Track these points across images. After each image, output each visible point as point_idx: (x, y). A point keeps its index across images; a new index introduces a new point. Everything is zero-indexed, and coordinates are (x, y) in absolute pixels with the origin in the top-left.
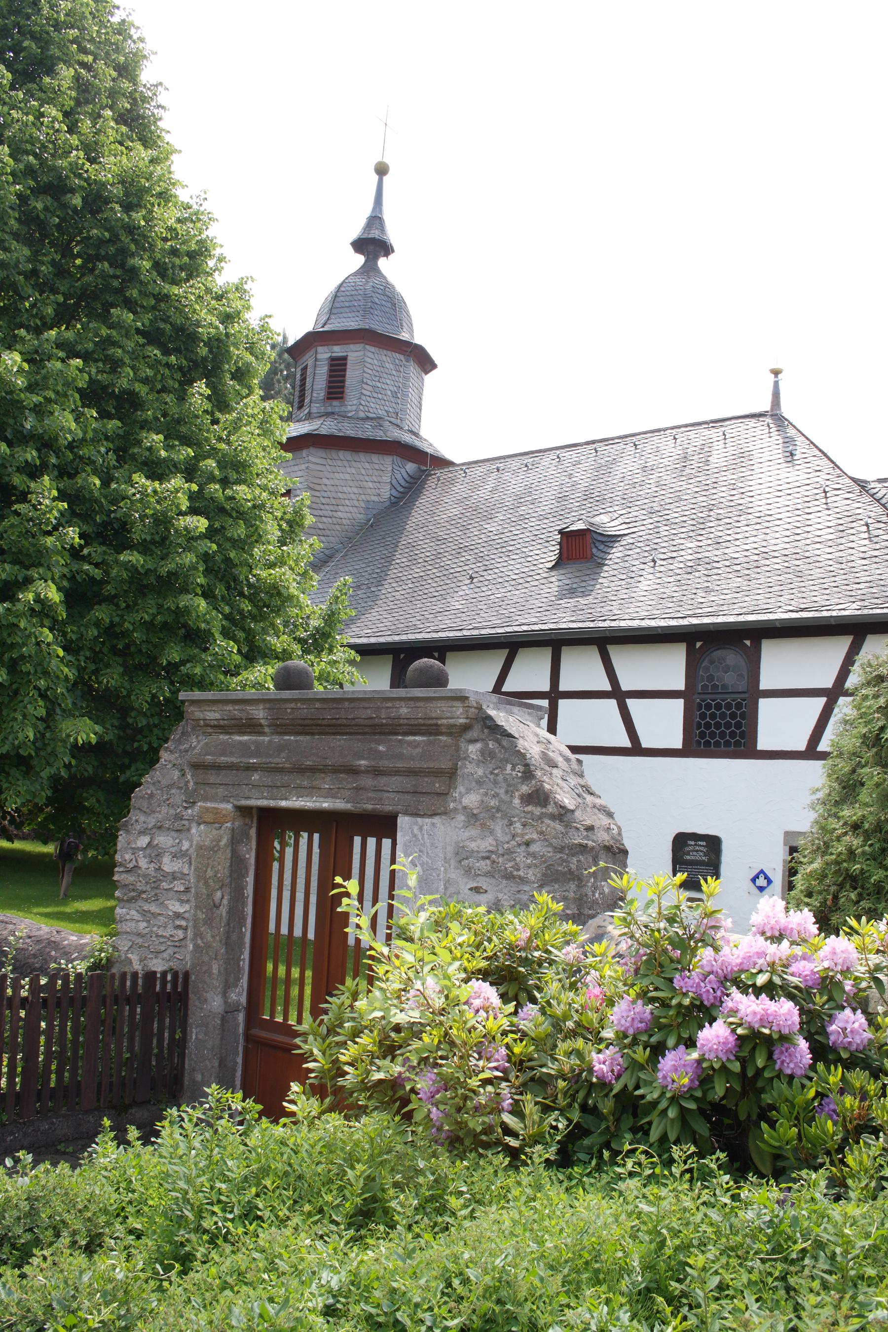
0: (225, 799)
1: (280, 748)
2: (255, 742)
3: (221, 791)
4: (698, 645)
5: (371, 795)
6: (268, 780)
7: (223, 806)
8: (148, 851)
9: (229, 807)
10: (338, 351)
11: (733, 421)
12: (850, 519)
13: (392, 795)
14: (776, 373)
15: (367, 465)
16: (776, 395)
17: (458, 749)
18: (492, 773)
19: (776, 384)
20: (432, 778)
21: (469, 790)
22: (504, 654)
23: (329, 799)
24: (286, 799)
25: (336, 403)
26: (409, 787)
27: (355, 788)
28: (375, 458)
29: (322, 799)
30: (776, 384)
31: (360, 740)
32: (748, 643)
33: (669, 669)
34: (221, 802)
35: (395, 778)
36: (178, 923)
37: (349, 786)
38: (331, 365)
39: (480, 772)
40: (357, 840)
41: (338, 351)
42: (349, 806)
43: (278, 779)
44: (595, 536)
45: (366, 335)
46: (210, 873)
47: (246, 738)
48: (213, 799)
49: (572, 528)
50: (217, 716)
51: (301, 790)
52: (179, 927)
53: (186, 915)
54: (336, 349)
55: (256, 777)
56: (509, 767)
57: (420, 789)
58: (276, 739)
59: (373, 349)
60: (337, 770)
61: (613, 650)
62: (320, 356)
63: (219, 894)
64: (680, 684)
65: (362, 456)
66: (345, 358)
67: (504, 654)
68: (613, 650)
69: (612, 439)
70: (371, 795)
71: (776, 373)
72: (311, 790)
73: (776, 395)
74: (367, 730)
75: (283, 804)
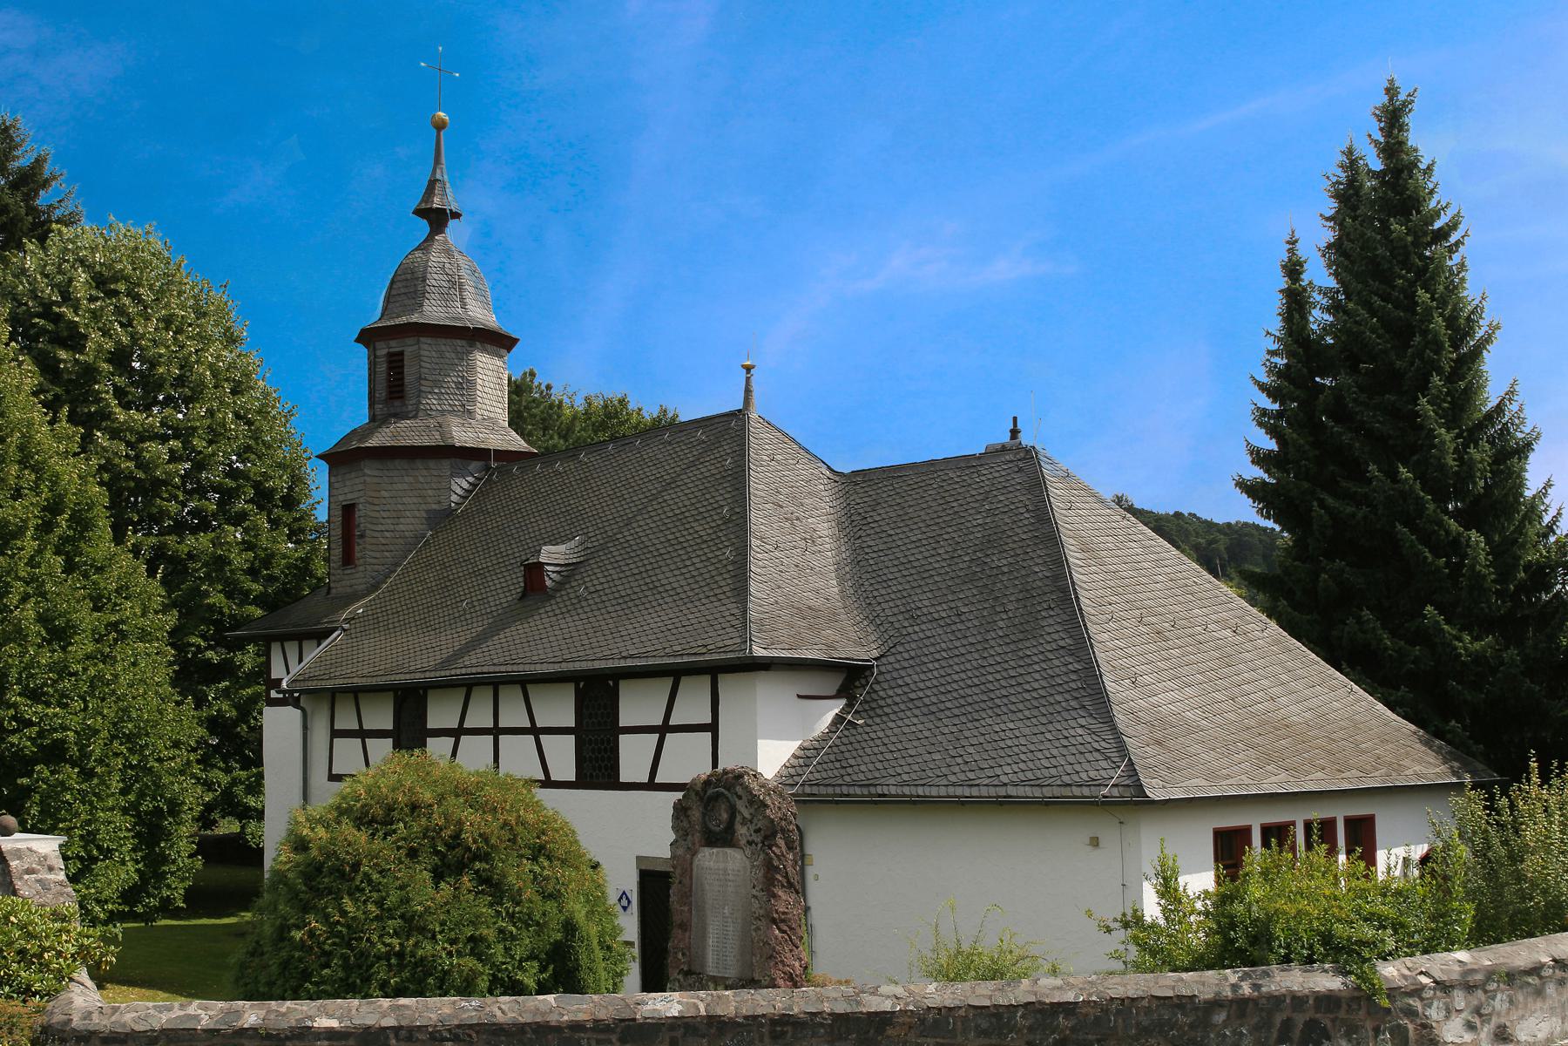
10: (395, 346)
15: (425, 473)
19: (748, 379)
22: (669, 682)
25: (397, 403)
28: (432, 464)
33: (559, 709)
38: (390, 362)
41: (395, 346)
45: (1430, 168)
54: (393, 343)
59: (429, 340)
61: (529, 687)
62: (379, 353)
64: (570, 722)
65: (419, 463)
66: (401, 353)
67: (669, 682)
68: (529, 687)
71: (748, 369)
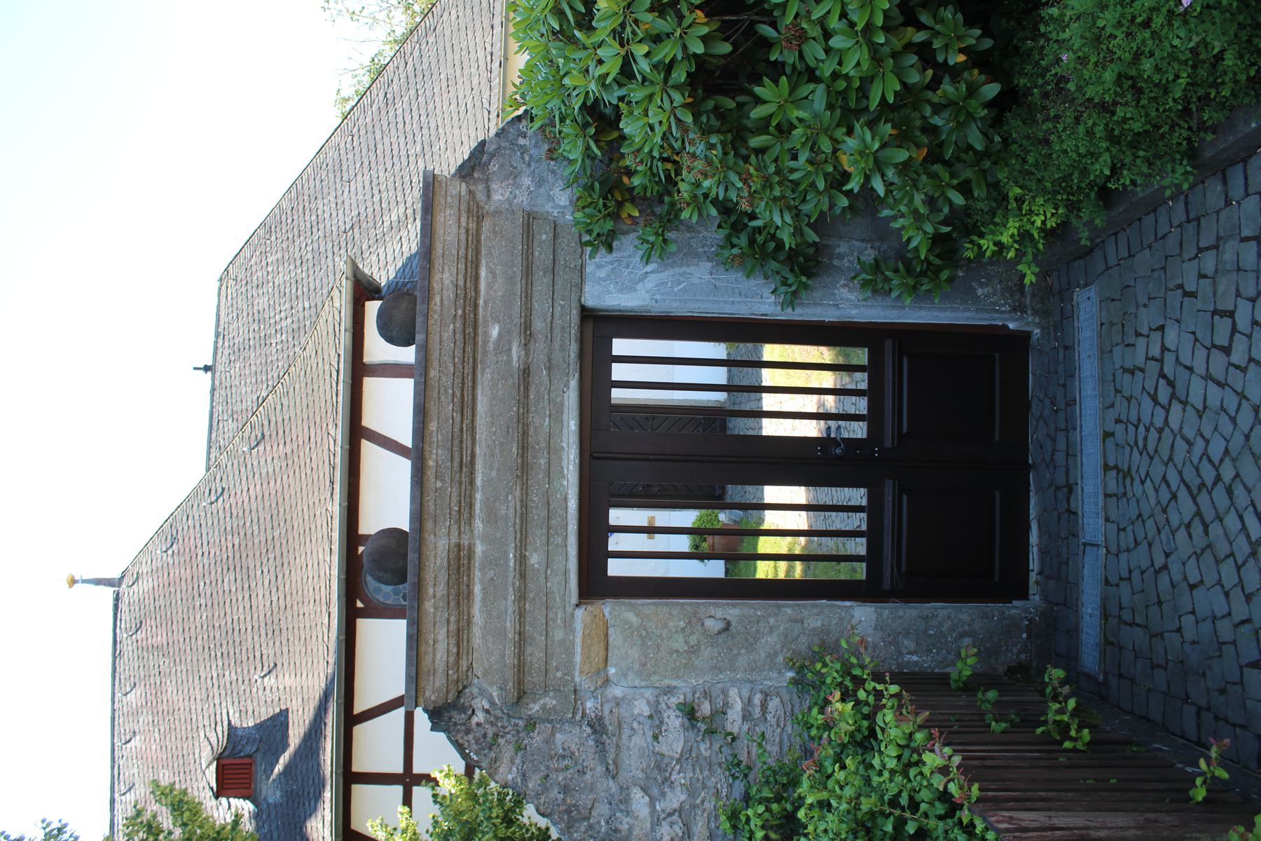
0: (568, 624)
1: (492, 517)
2: (483, 569)
3: (559, 635)
4: (359, 604)
5: (557, 345)
6: (537, 537)
7: (579, 626)
8: (655, 791)
9: (580, 613)
11: (118, 631)
12: (243, 470)
13: (558, 310)
14: (73, 582)
16: (98, 582)
17: (497, 213)
18: (529, 165)
19: (85, 581)
20: (536, 243)
21: (550, 198)
23: (565, 417)
24: (566, 499)
26: (547, 280)
27: (549, 369)
29: (565, 432)
30: (85, 581)
31: (484, 369)
32: (361, 549)
34: (573, 631)
35: (536, 305)
36: (757, 711)
37: (546, 379)
39: (526, 181)
40: (618, 395)
42: (574, 383)
43: (538, 513)
44: (226, 754)
46: (679, 644)
47: (477, 589)
48: (570, 652)
49: (214, 785)
50: (442, 633)
51: (553, 471)
52: (764, 706)
53: (746, 694)
55: (534, 559)
56: (522, 141)
57: (549, 263)
58: (479, 525)
60: (524, 403)
63: (709, 623)
67: (367, 446)
69: (113, 777)
70: (557, 345)
72: (553, 450)
73: (98, 582)
74: (469, 349)
75: (573, 504)
